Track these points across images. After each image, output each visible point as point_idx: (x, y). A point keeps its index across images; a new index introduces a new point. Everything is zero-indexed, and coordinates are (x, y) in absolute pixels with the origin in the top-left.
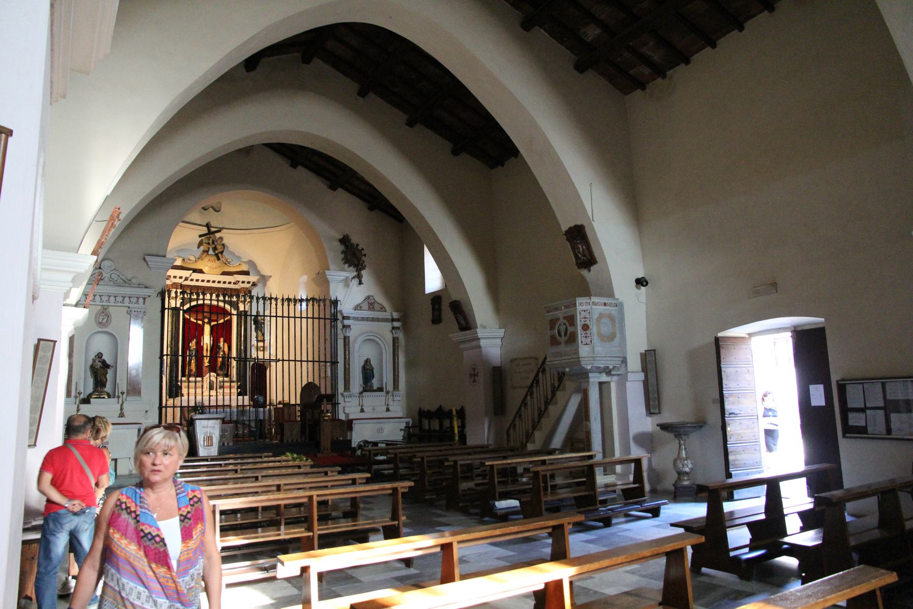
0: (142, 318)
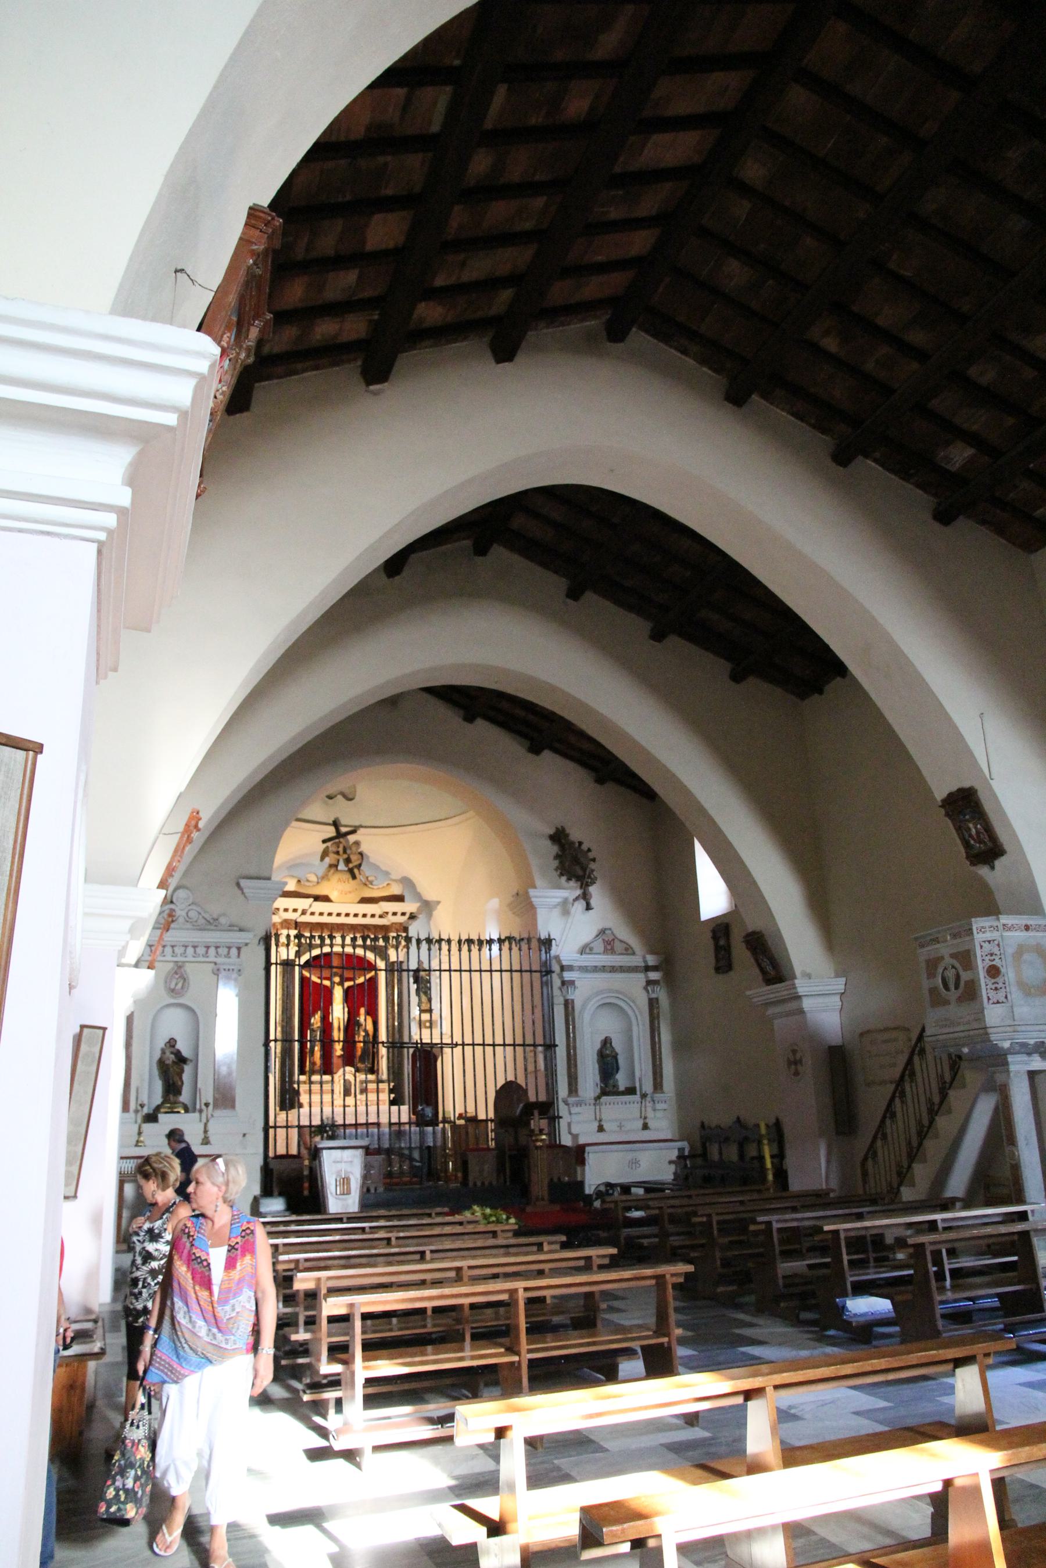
0: (236, 980)
